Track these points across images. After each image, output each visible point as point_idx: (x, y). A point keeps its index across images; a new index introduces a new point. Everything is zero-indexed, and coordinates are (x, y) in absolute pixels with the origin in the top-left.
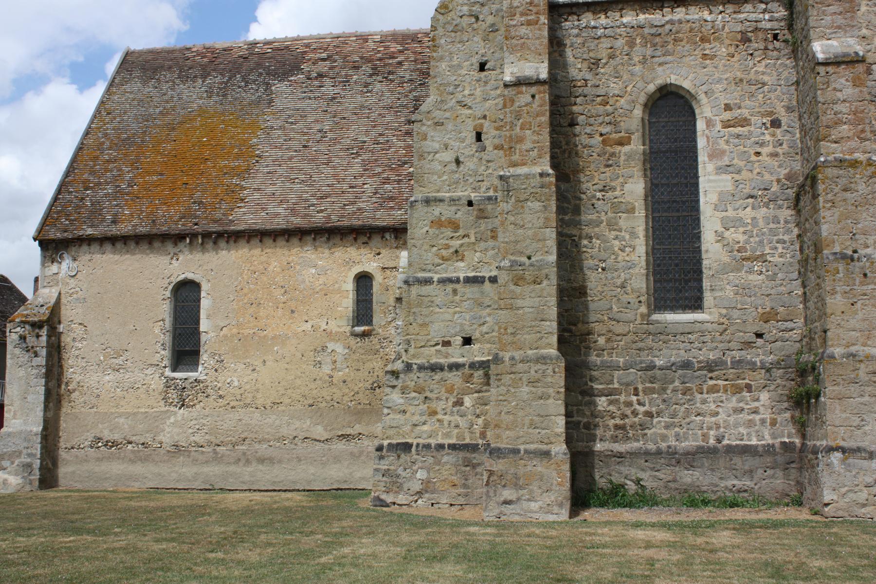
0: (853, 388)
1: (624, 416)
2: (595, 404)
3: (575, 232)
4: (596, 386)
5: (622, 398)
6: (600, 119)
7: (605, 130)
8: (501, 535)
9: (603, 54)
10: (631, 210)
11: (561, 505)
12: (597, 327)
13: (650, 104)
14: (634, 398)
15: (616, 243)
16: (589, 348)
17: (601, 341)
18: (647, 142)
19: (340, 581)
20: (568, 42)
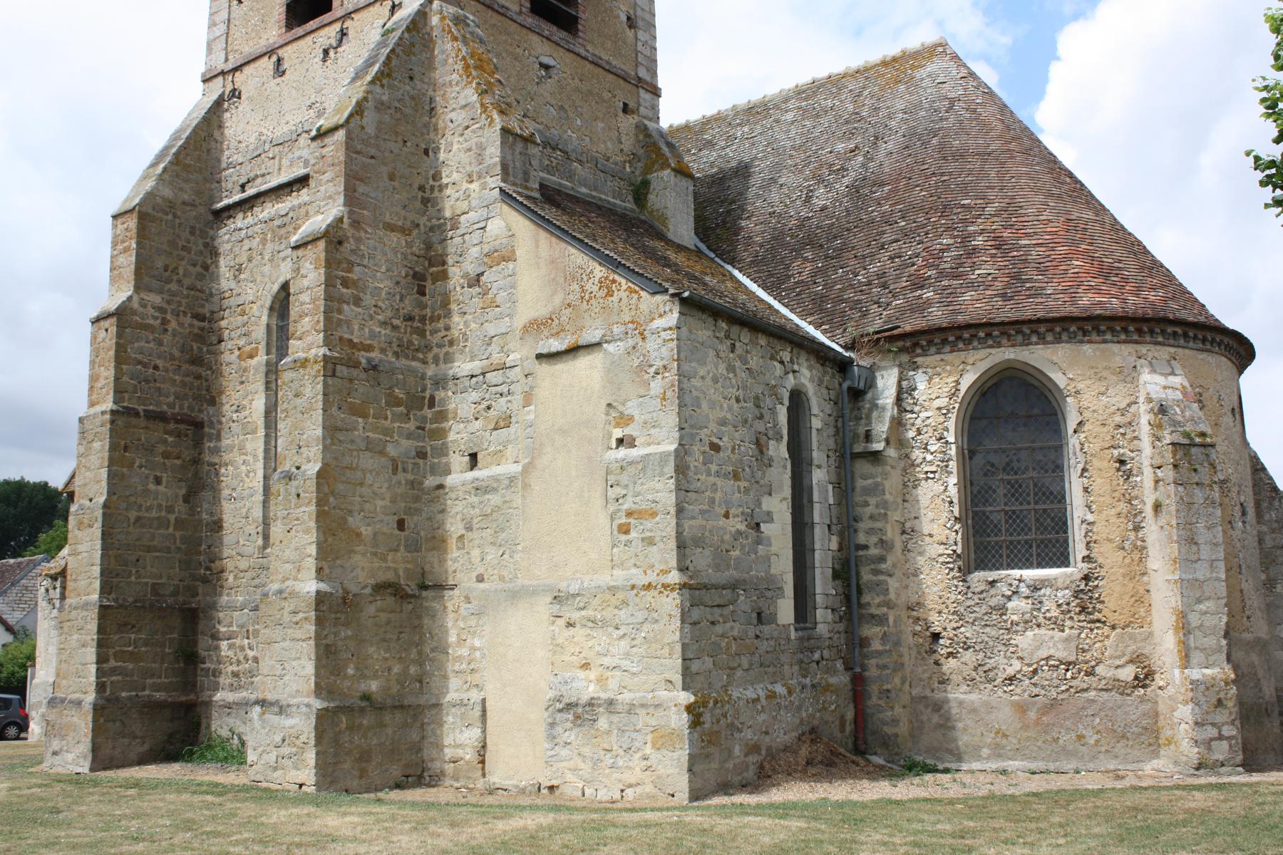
0: (279, 630)
1: (239, 662)
2: (217, 648)
3: (216, 460)
4: (223, 629)
5: (238, 642)
6: (239, 332)
7: (241, 342)
8: (1225, 801)
9: (243, 258)
10: (254, 432)
11: (85, 757)
12: (229, 564)
13: (277, 306)
14: (246, 641)
15: (243, 468)
16: (222, 587)
17: (231, 578)
18: (274, 350)
19: (984, 850)
20: (221, 250)
